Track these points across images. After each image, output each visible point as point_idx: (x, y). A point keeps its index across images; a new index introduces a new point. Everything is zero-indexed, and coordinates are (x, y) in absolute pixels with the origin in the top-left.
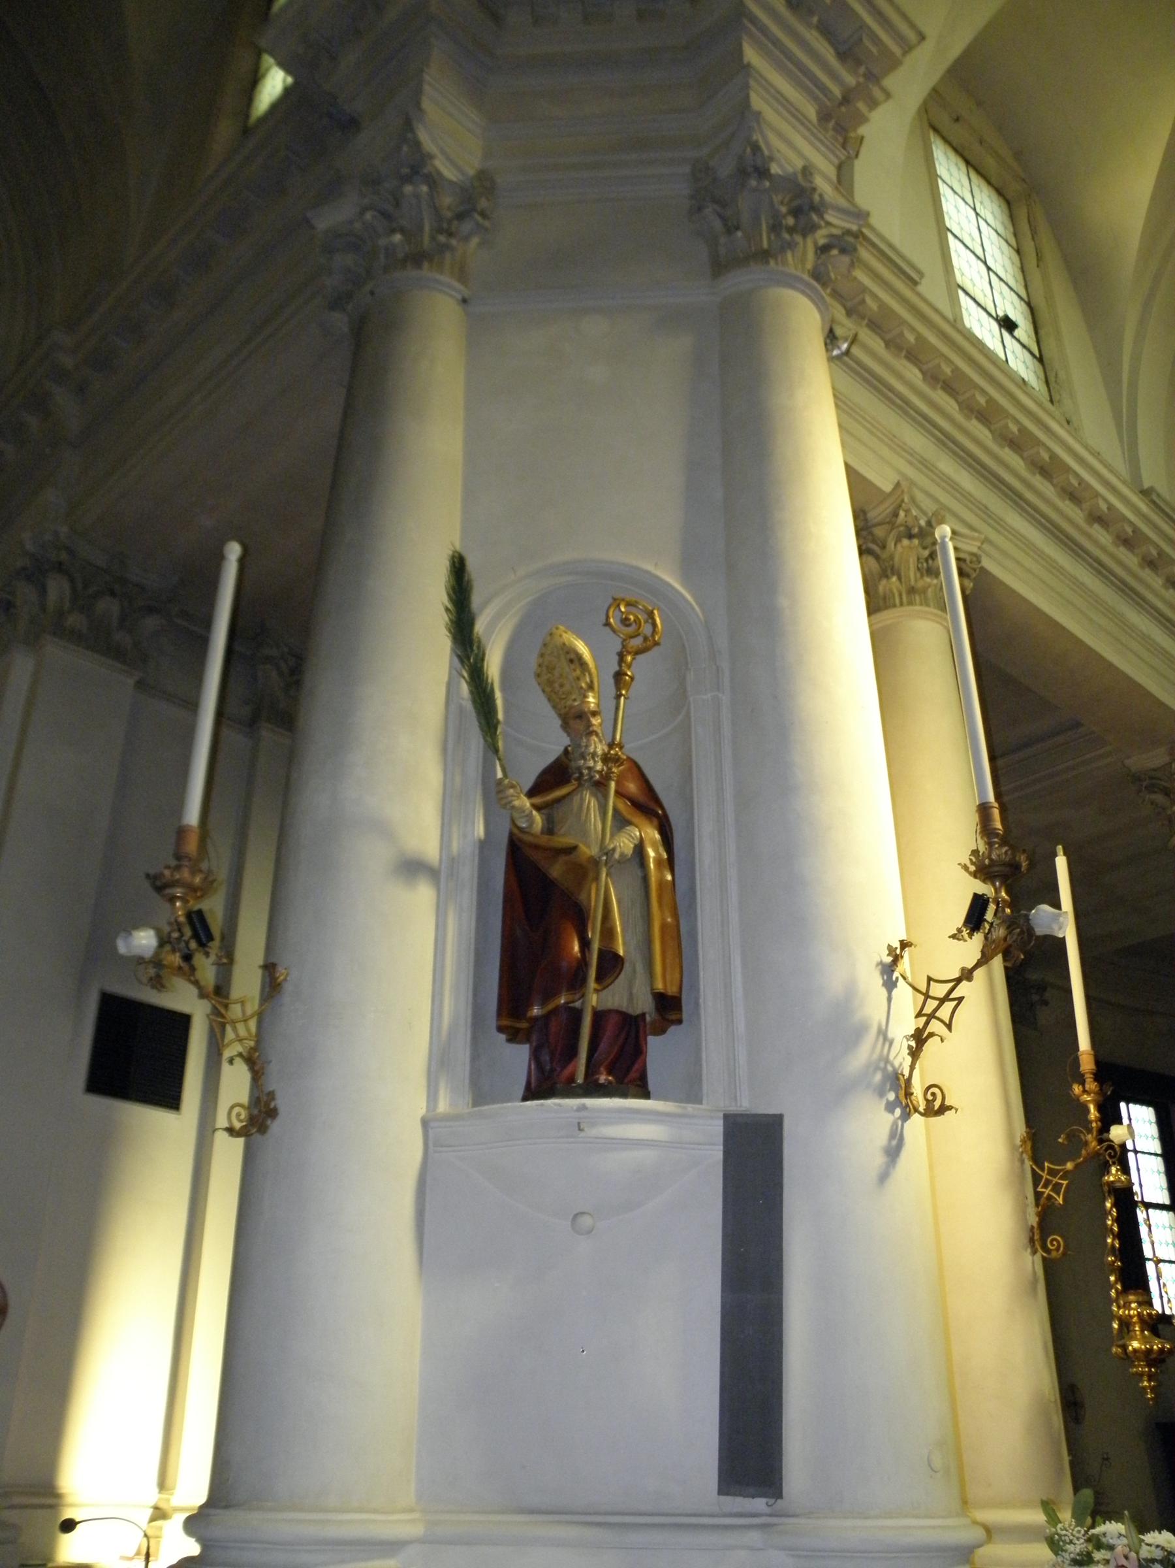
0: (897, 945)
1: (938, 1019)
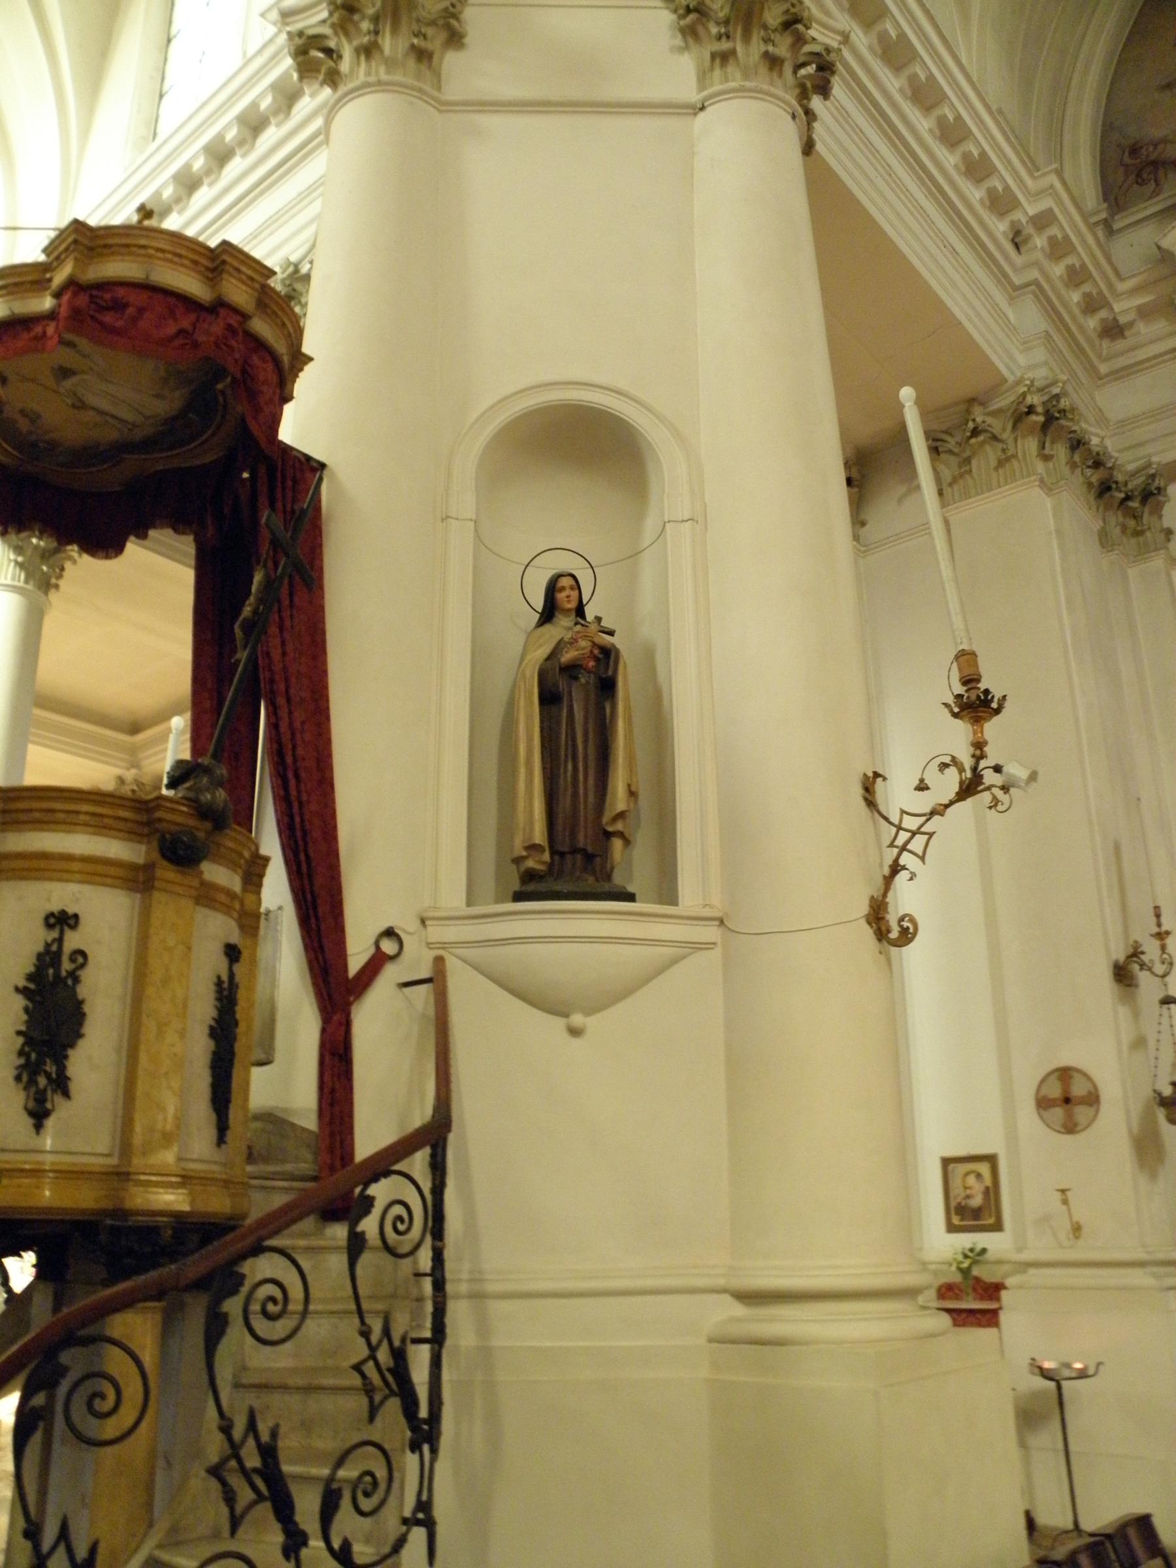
0: (870, 774)
1: (910, 852)
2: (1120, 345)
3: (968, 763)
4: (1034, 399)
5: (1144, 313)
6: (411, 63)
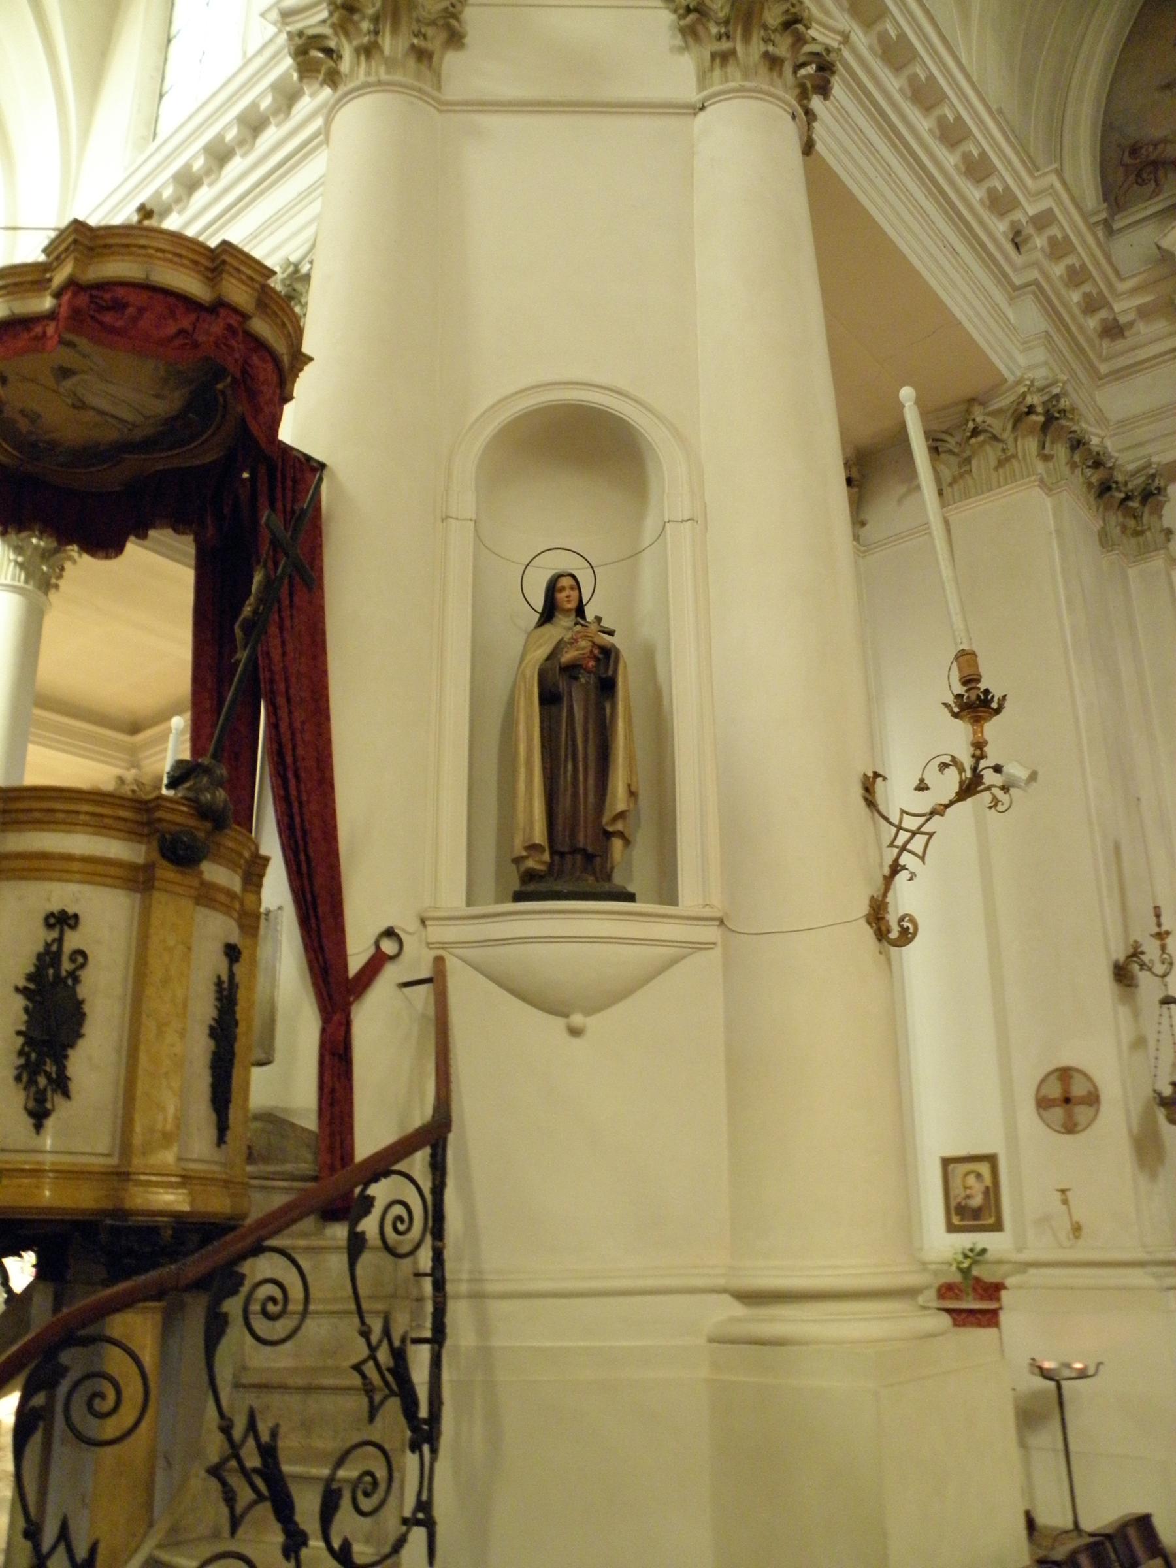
0: (870, 774)
1: (910, 852)
2: (1120, 345)
3: (968, 763)
4: (1034, 399)
5: (1144, 313)
6: (411, 63)
